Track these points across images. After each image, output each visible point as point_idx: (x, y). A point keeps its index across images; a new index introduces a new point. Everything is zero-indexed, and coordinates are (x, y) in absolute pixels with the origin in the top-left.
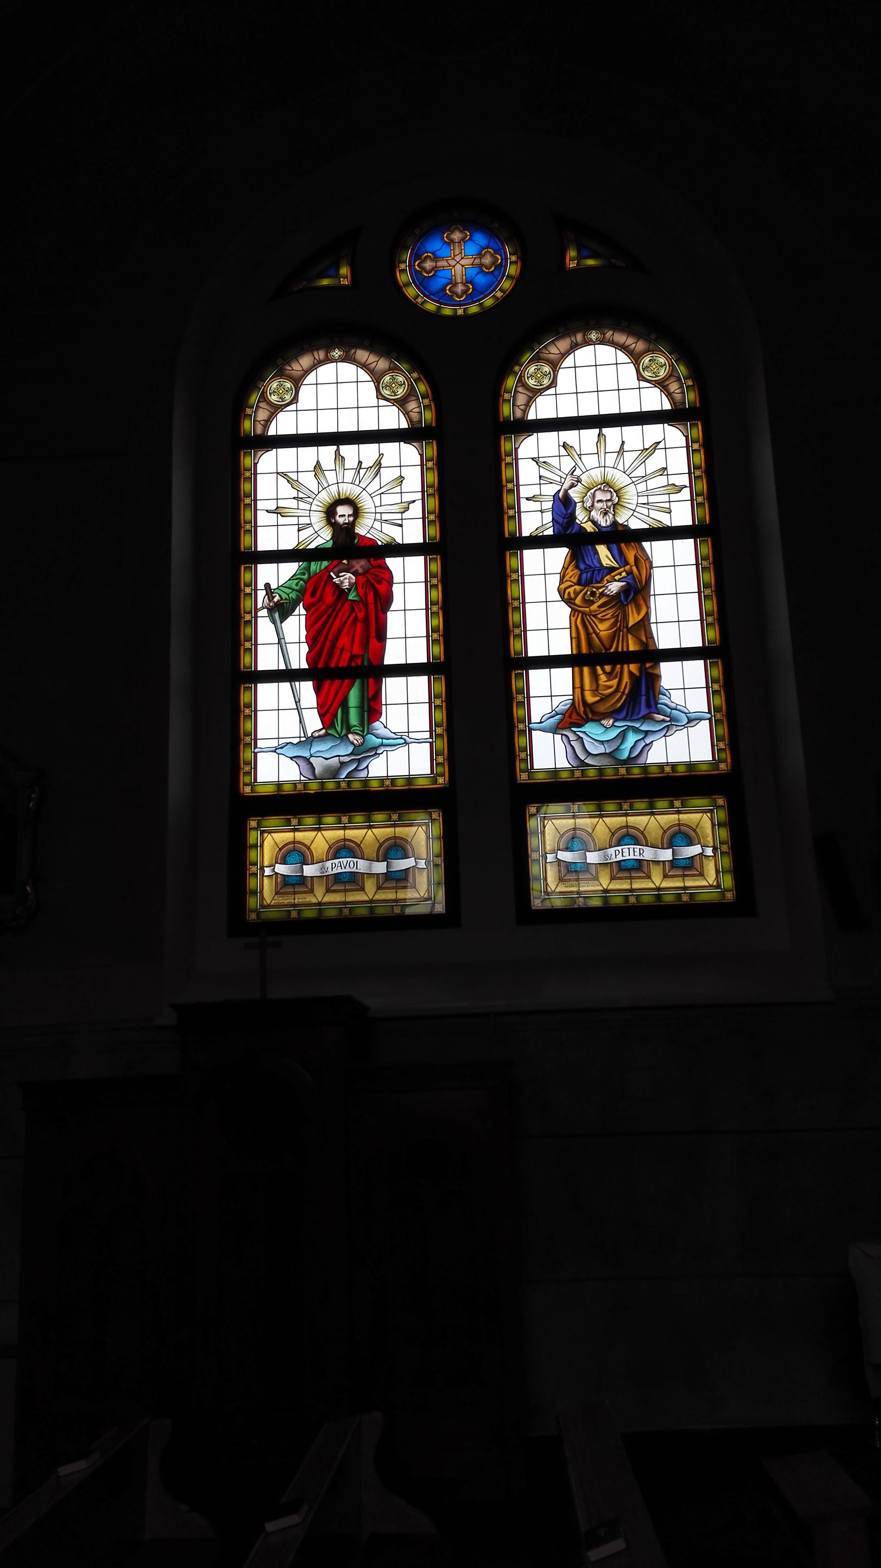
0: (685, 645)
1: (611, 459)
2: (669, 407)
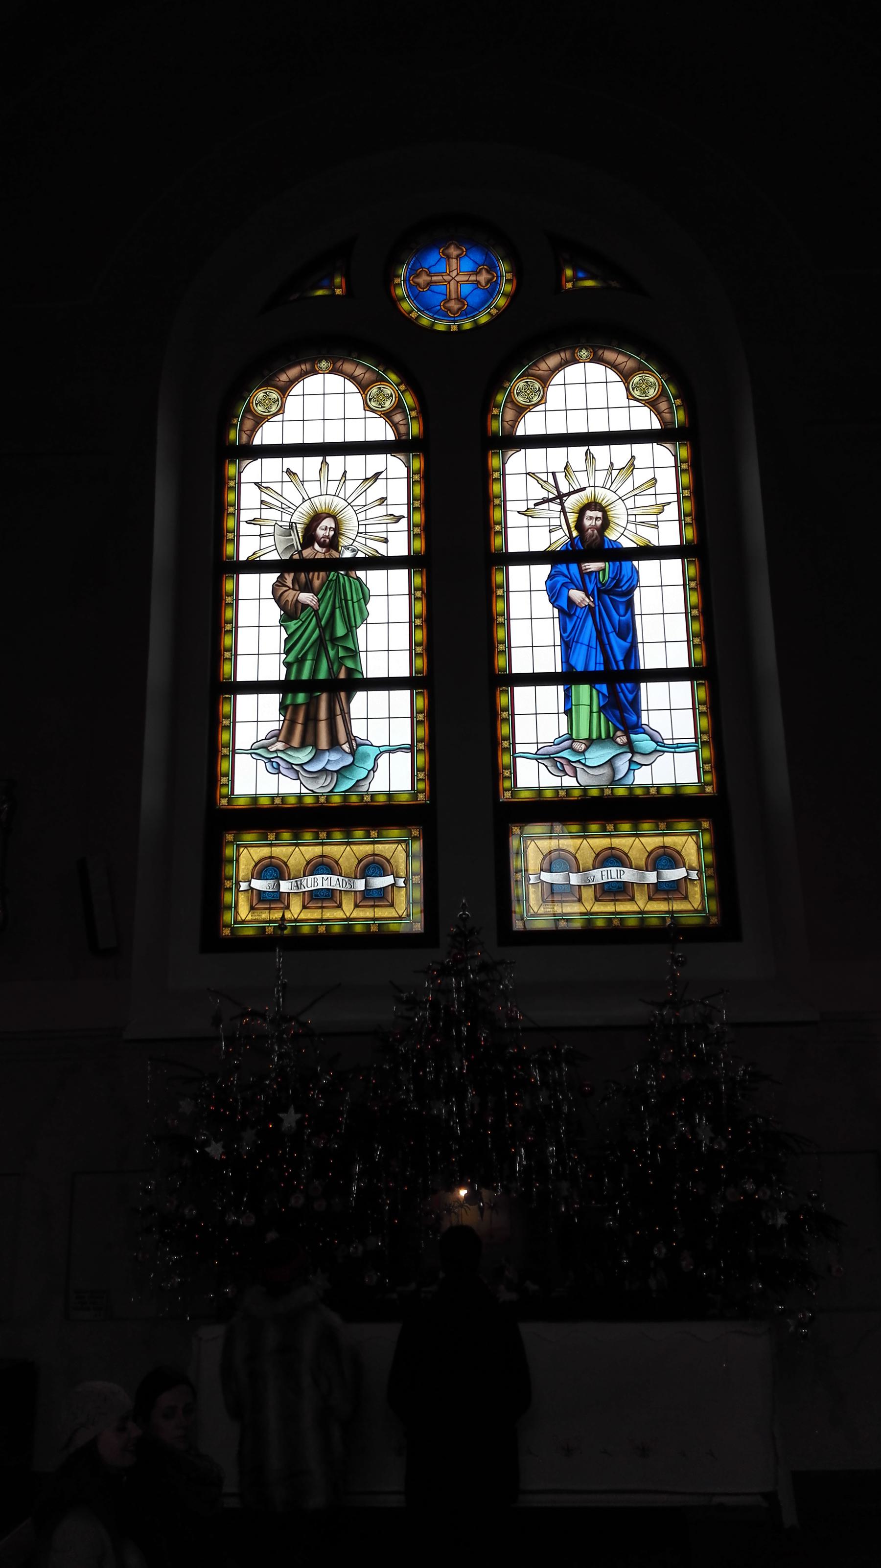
2: (659, 427)
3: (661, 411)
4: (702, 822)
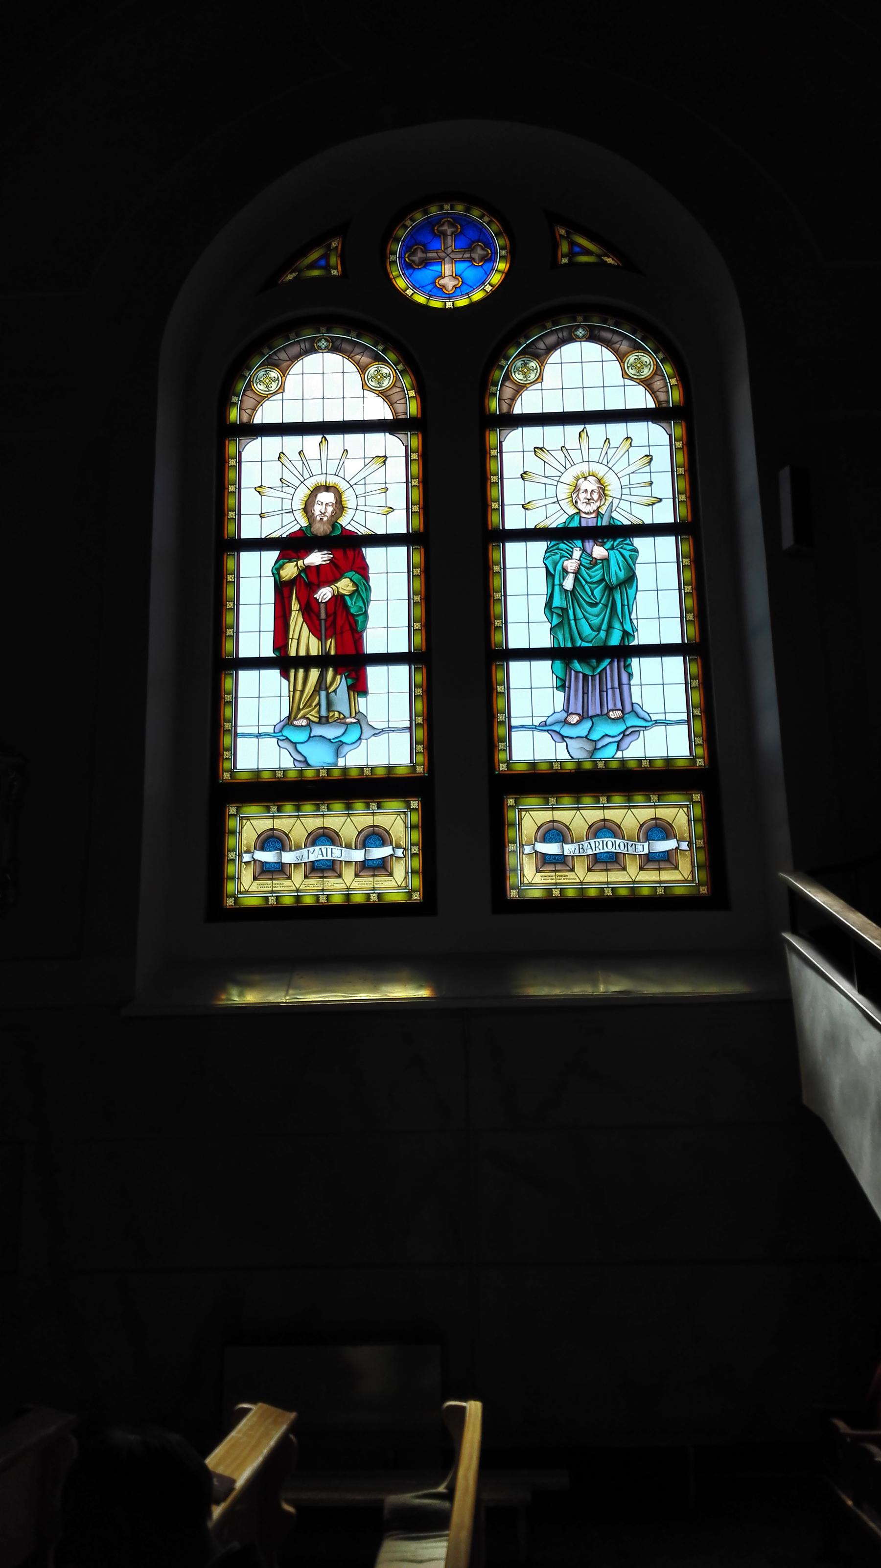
0: (665, 641)
2: (653, 406)
3: (656, 390)
4: (411, 802)
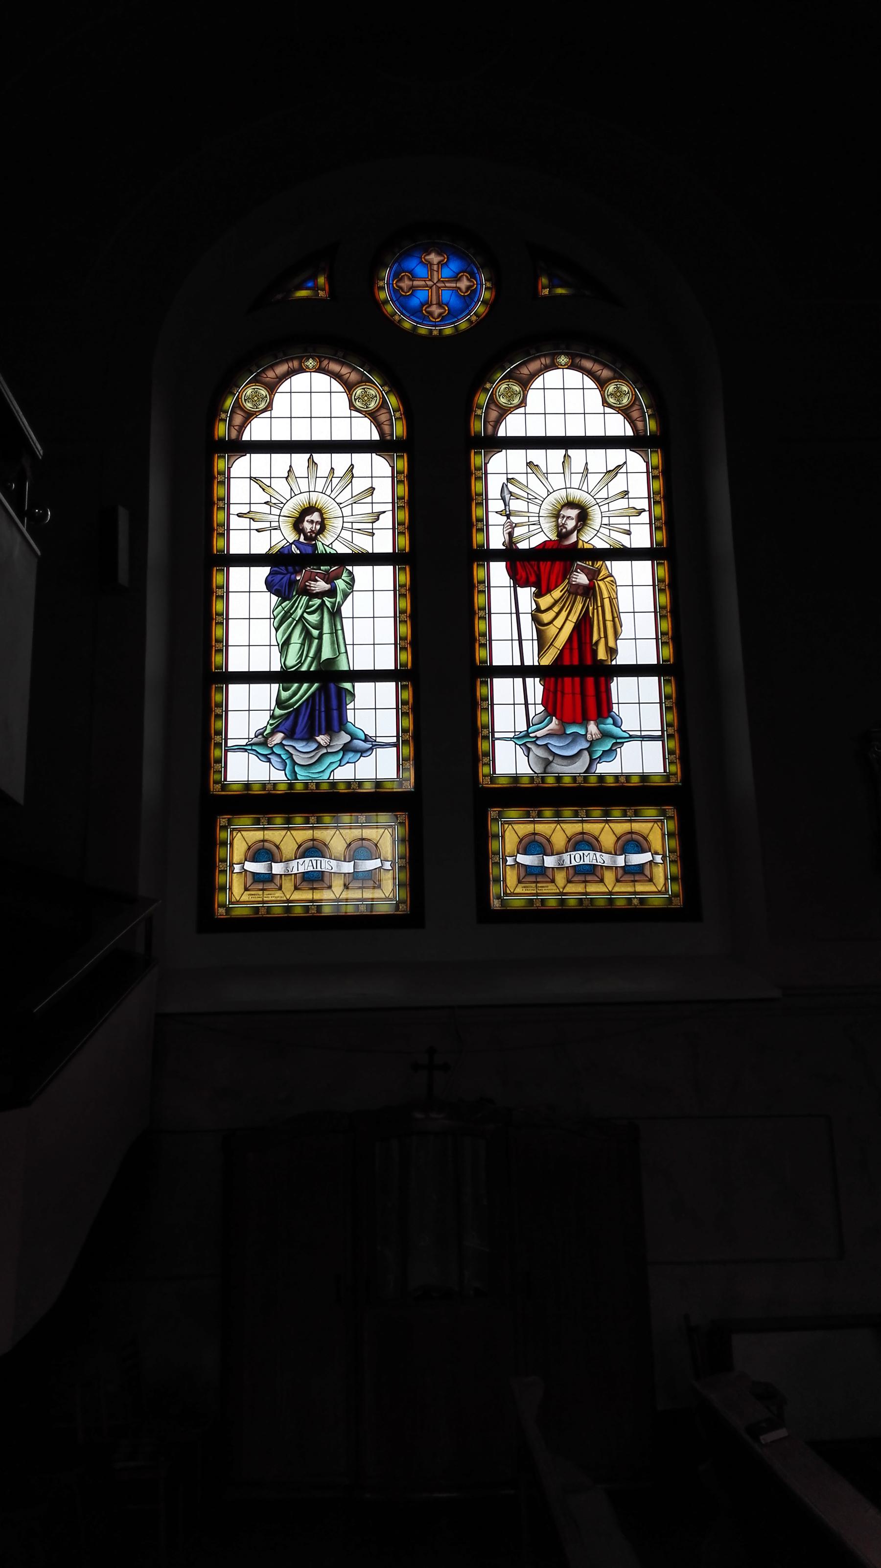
1: (576, 480)
2: (378, 438)
